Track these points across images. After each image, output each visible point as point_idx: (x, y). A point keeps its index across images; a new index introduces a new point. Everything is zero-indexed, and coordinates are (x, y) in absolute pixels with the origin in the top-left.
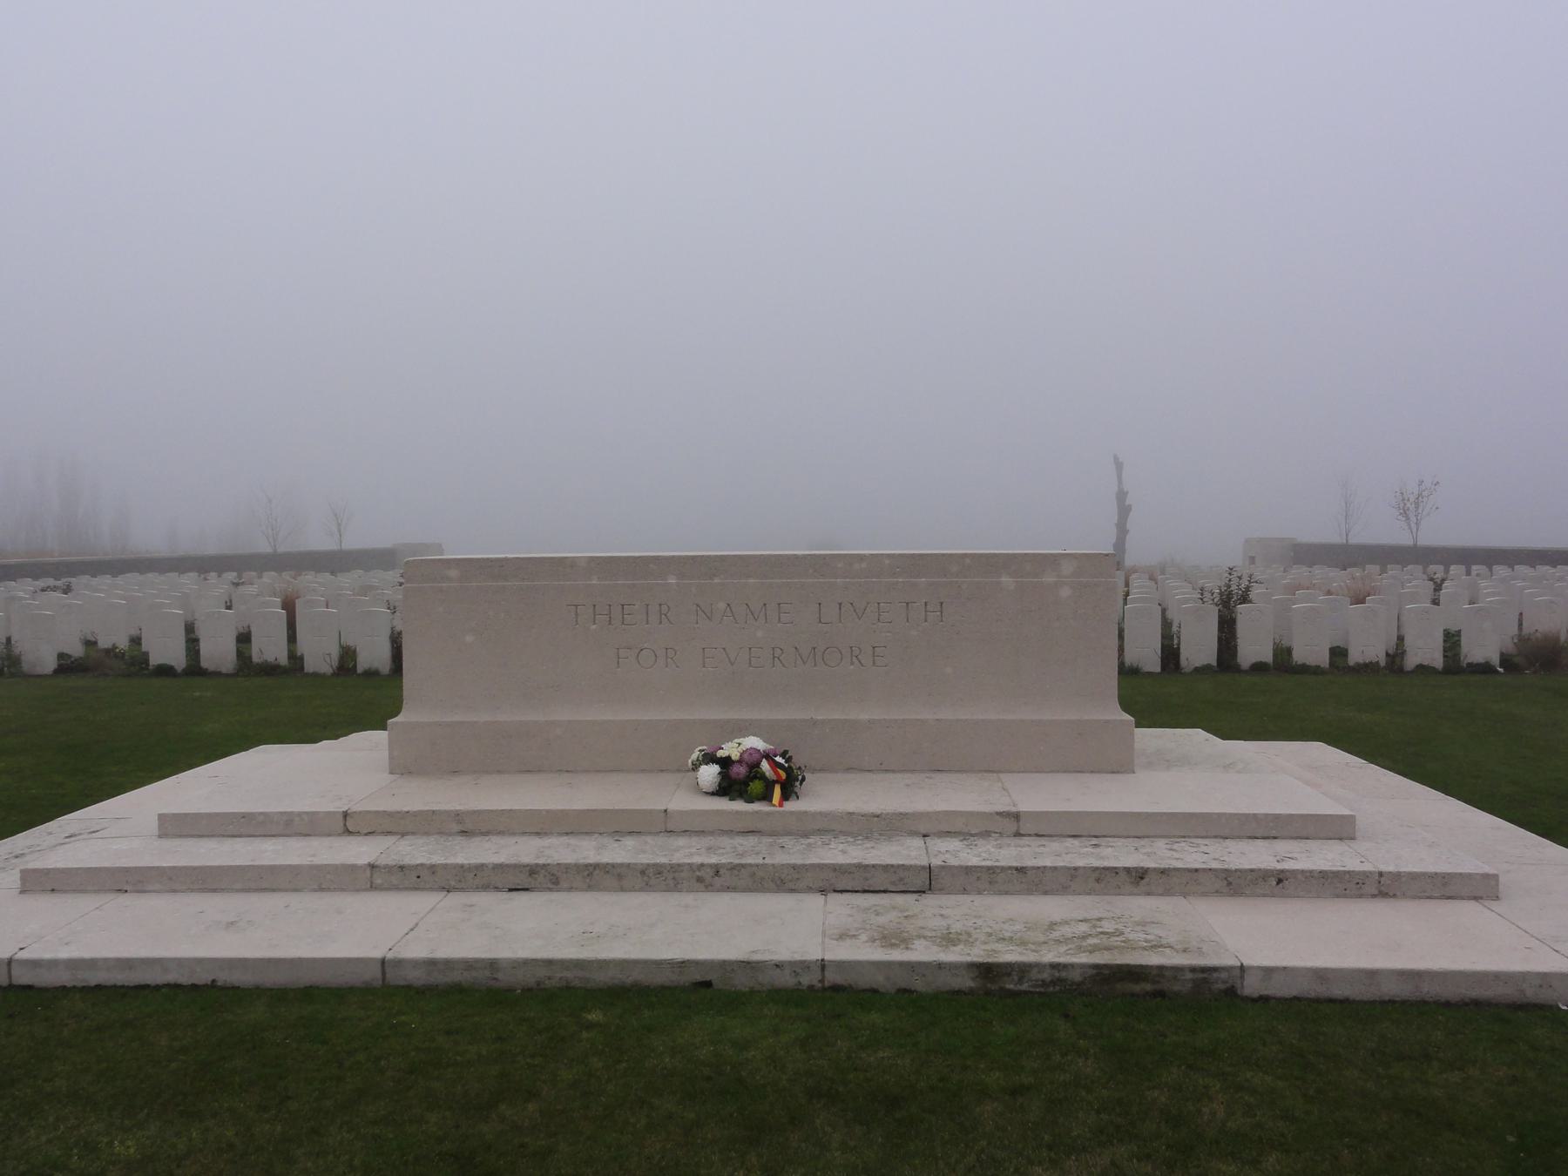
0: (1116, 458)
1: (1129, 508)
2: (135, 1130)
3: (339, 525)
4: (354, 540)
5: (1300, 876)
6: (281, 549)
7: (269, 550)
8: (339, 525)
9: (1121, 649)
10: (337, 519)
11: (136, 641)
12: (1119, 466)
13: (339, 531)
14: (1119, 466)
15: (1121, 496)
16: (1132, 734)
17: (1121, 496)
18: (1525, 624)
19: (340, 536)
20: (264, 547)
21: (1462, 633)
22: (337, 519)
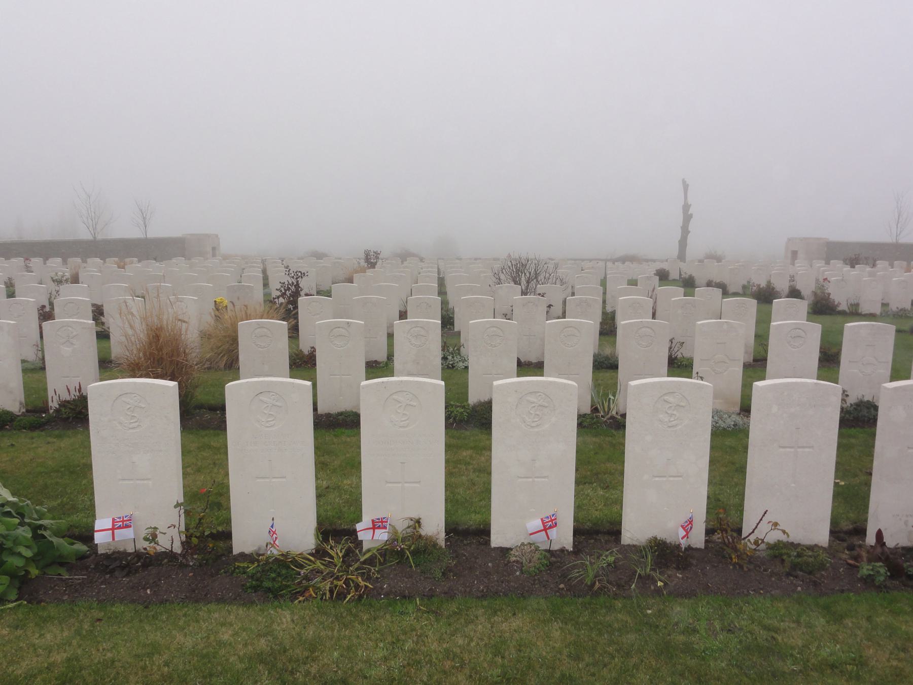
0: (684, 182)
1: (691, 216)
2: (358, 480)
3: (144, 218)
4: (156, 231)
5: (566, 552)
6: (100, 237)
7: (91, 238)
8: (144, 218)
9: (604, 302)
10: (143, 214)
11: (769, 282)
12: (686, 187)
13: (145, 223)
14: (686, 187)
15: (686, 207)
16: (108, 517)
17: (686, 207)
18: (690, 239)
19: (146, 227)
20: (84, 234)
21: (318, 354)
22: (143, 214)
